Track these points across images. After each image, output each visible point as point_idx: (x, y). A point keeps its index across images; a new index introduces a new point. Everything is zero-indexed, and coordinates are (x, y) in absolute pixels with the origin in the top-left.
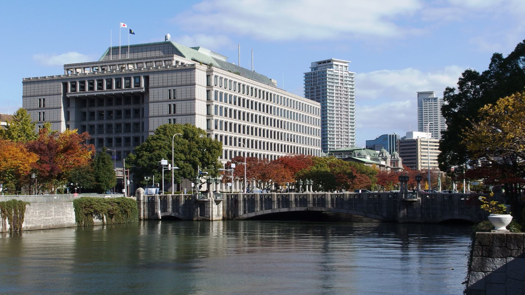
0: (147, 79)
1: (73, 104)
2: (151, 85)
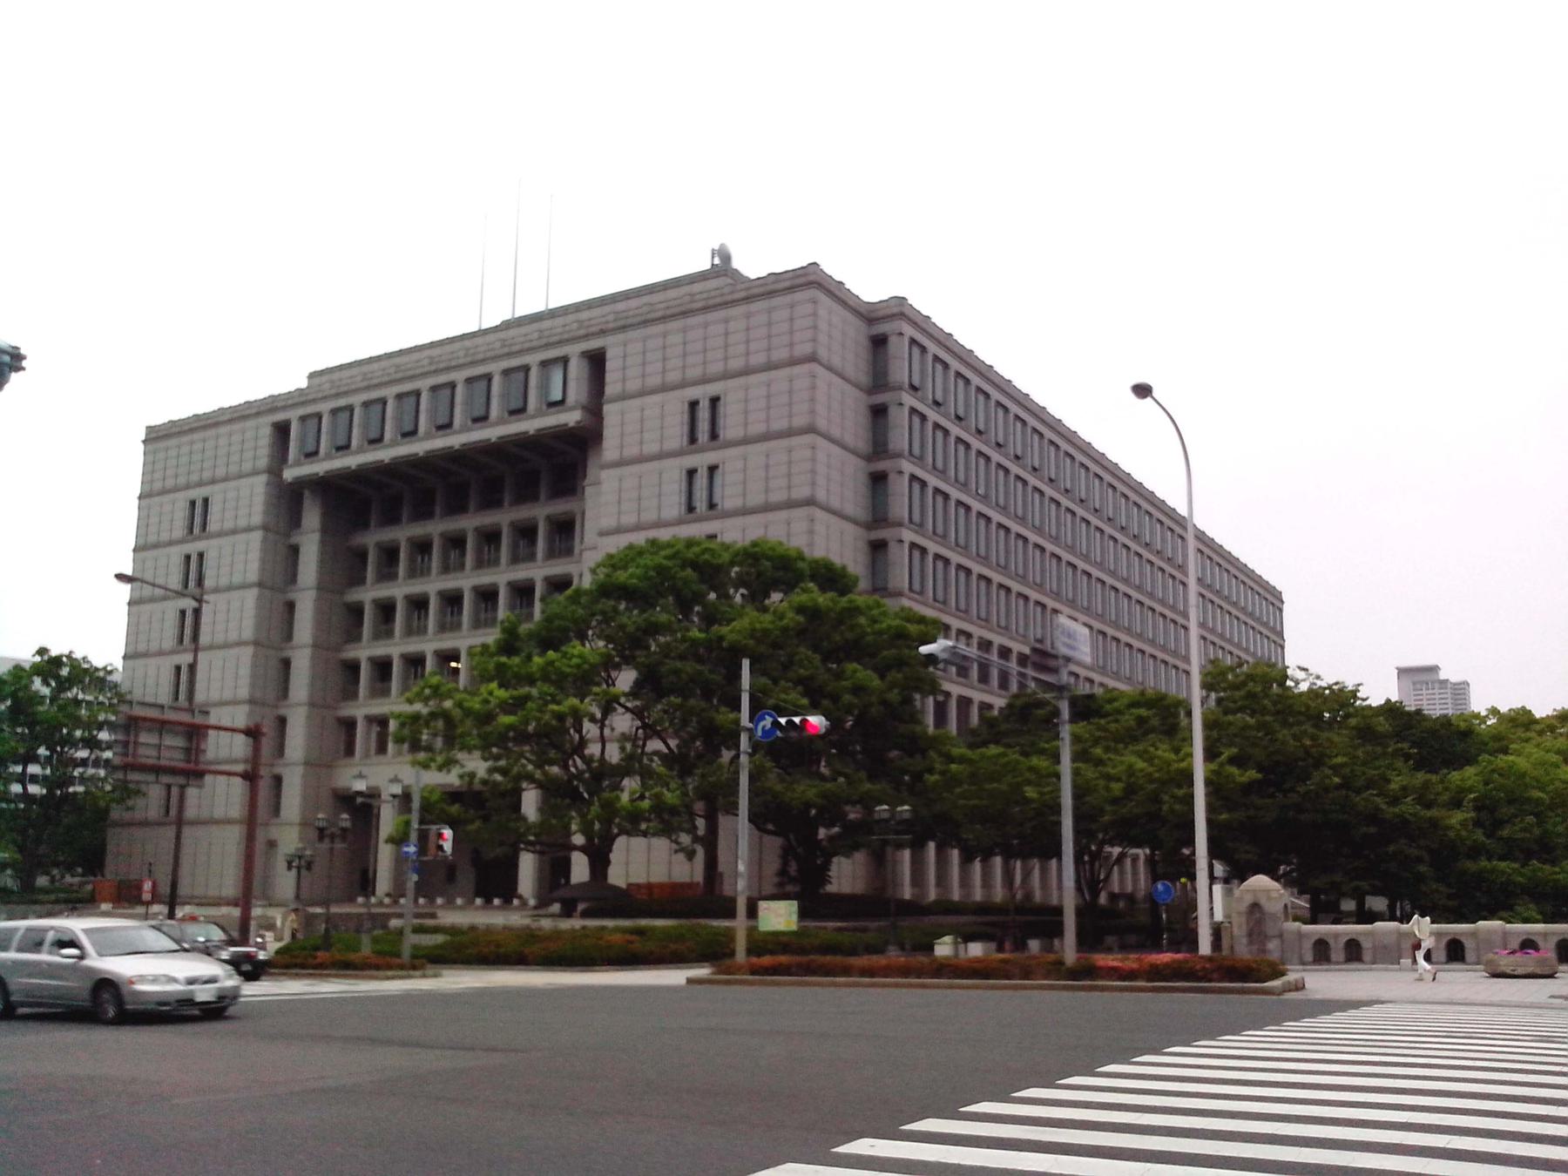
0: (597, 361)
1: (312, 518)
2: (611, 389)
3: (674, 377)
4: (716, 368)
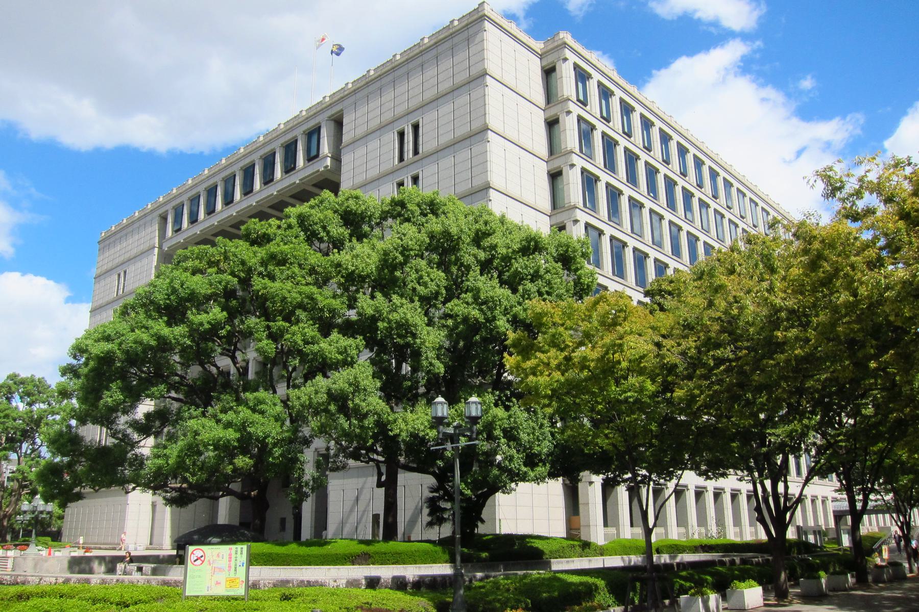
2: (346, 138)
3: (388, 116)
4: (414, 103)
